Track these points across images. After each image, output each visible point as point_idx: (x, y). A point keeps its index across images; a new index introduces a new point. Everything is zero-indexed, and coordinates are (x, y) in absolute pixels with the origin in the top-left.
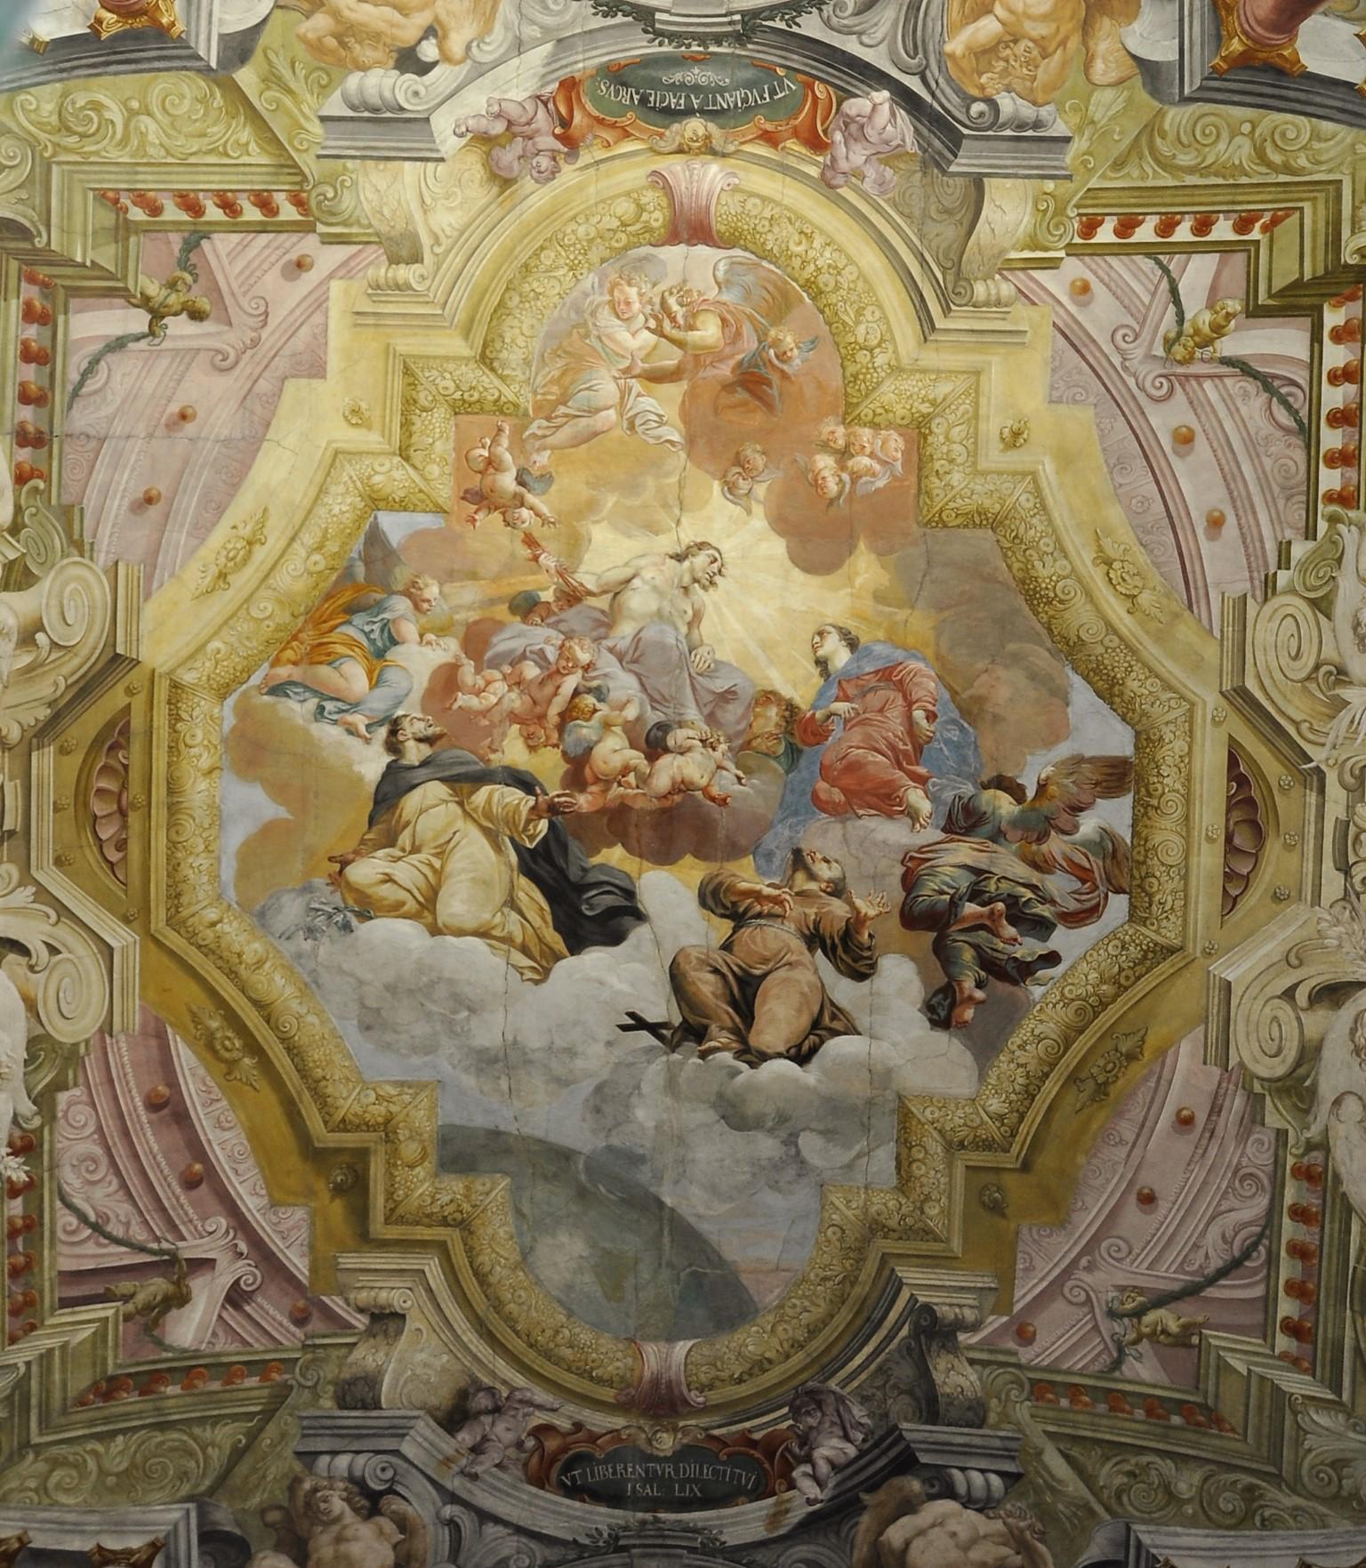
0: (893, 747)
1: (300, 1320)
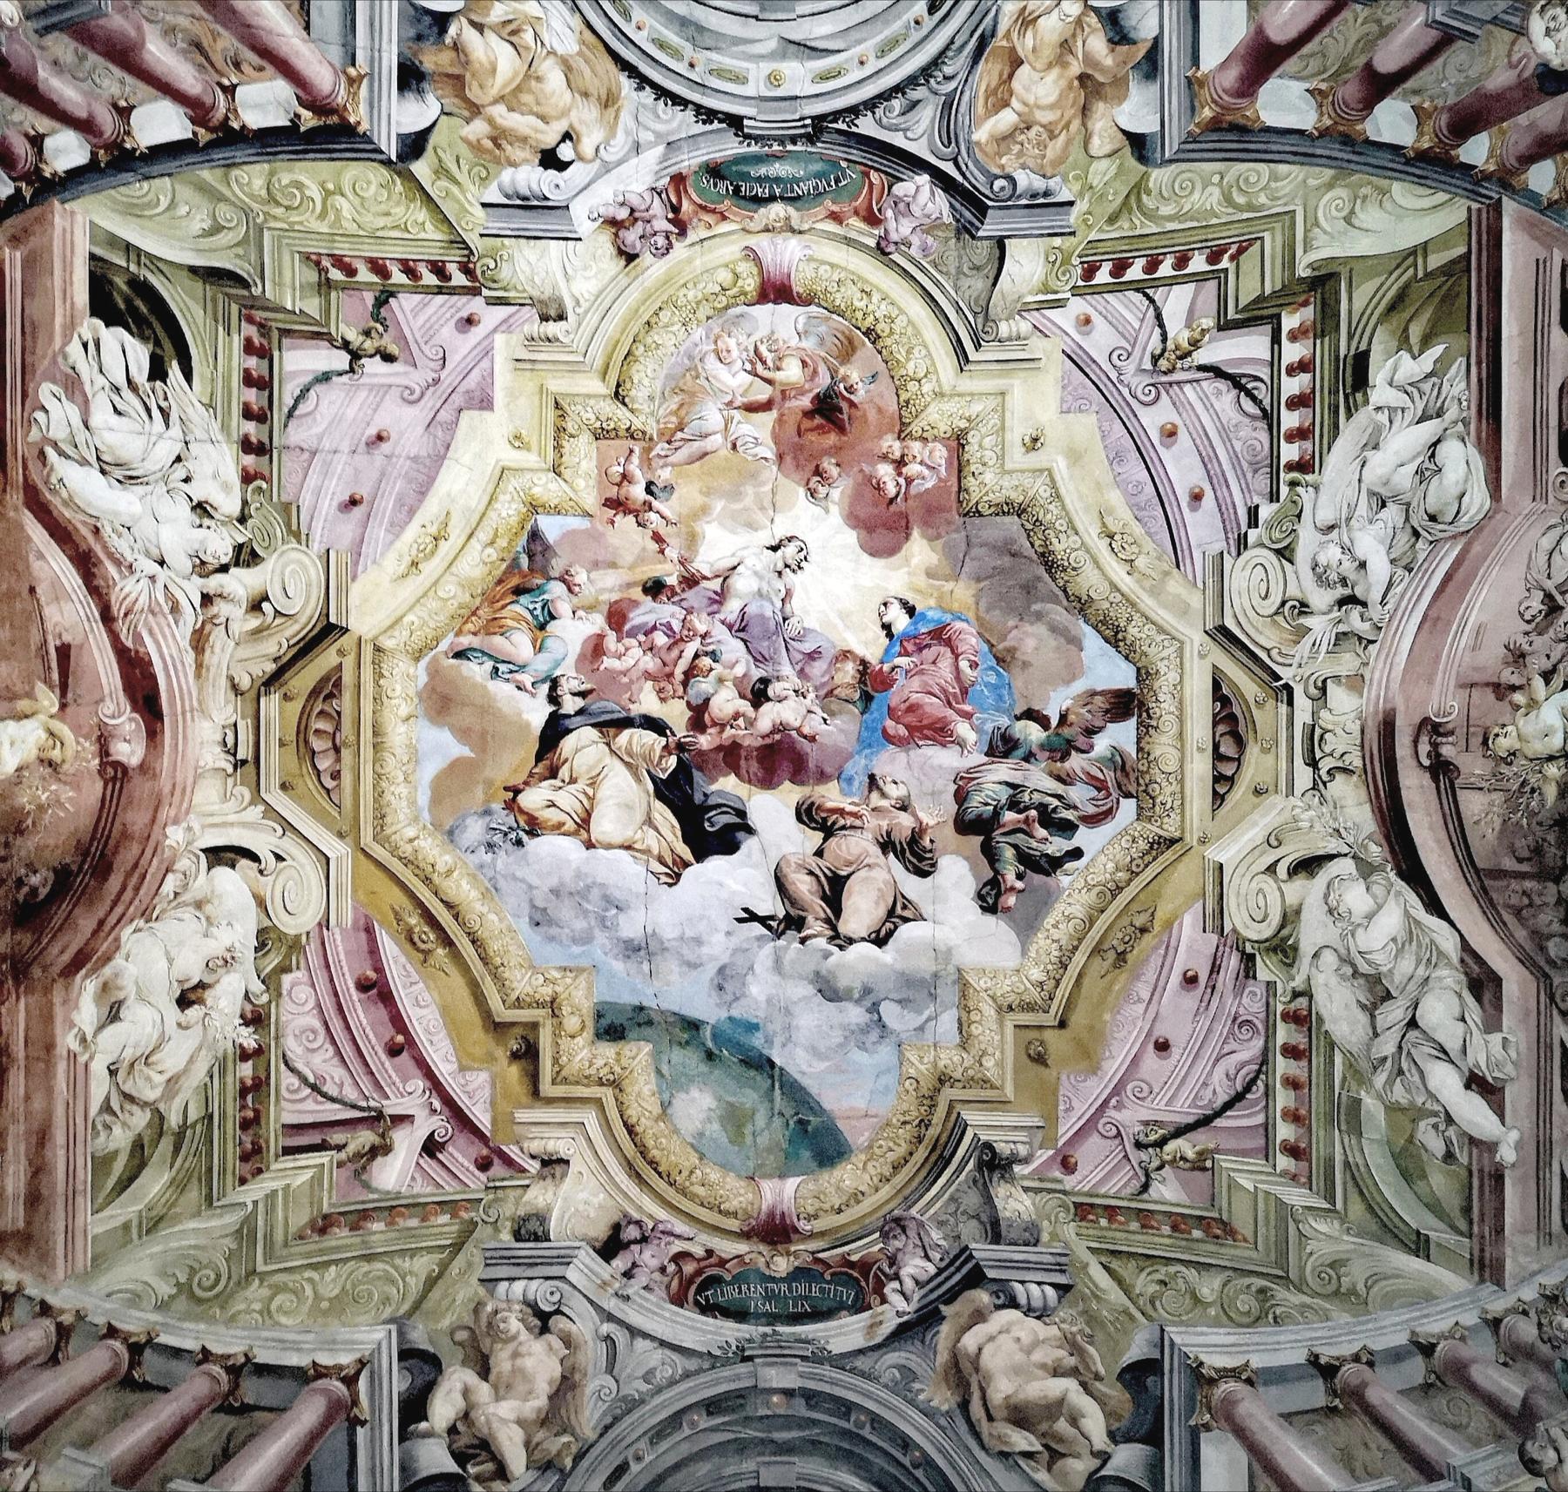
0: (944, 691)
1: (484, 1165)
